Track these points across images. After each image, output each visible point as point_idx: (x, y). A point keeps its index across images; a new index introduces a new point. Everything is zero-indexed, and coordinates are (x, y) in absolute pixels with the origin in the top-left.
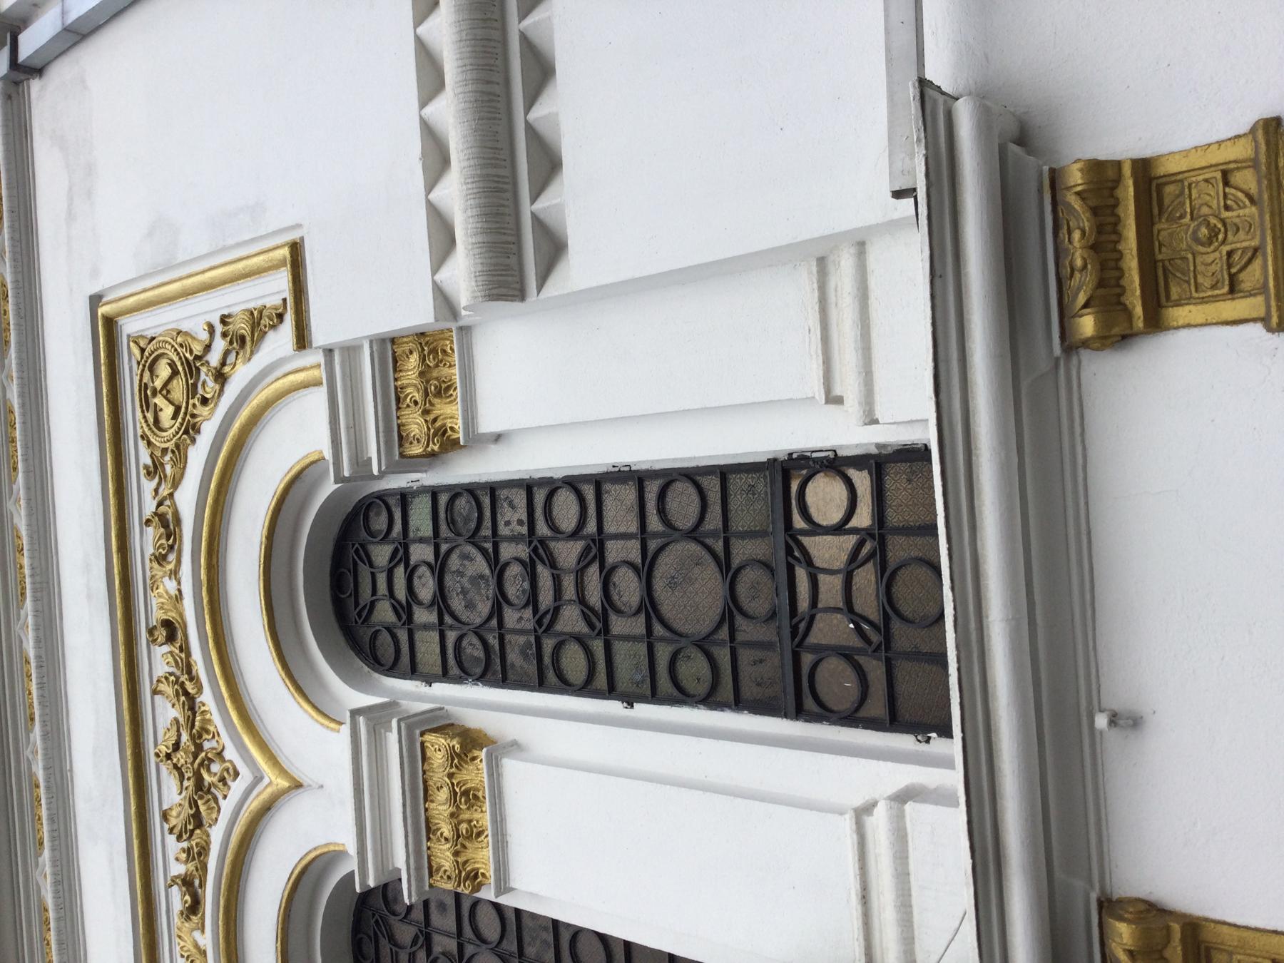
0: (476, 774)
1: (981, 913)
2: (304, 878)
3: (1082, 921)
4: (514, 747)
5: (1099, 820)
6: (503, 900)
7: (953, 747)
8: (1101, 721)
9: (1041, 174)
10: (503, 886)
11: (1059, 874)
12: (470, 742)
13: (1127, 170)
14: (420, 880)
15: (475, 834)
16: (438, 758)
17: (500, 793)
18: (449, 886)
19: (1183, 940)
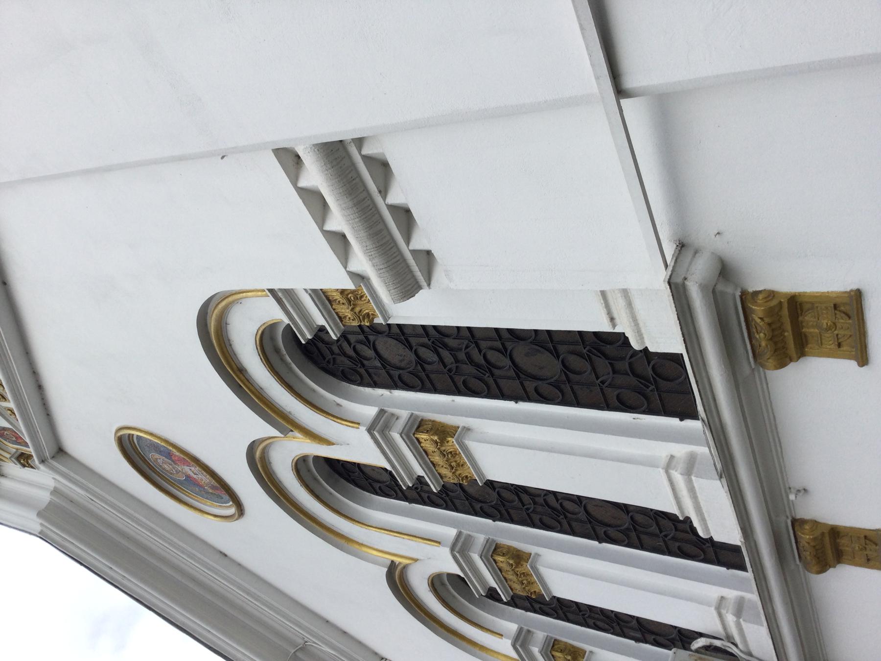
0: (452, 443)
1: (705, 401)
2: (264, 341)
3: (786, 536)
4: (467, 429)
5: (772, 410)
6: (390, 322)
7: (749, 575)
8: (792, 497)
9: (787, 523)
10: (386, 316)
11: (774, 518)
12: (443, 432)
13: (794, 355)
14: (336, 325)
15: (454, 454)
16: (430, 447)
17: (375, 292)
18: (355, 323)
19: (789, 308)
